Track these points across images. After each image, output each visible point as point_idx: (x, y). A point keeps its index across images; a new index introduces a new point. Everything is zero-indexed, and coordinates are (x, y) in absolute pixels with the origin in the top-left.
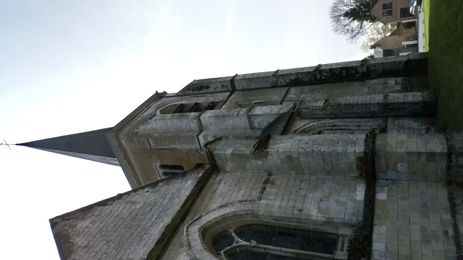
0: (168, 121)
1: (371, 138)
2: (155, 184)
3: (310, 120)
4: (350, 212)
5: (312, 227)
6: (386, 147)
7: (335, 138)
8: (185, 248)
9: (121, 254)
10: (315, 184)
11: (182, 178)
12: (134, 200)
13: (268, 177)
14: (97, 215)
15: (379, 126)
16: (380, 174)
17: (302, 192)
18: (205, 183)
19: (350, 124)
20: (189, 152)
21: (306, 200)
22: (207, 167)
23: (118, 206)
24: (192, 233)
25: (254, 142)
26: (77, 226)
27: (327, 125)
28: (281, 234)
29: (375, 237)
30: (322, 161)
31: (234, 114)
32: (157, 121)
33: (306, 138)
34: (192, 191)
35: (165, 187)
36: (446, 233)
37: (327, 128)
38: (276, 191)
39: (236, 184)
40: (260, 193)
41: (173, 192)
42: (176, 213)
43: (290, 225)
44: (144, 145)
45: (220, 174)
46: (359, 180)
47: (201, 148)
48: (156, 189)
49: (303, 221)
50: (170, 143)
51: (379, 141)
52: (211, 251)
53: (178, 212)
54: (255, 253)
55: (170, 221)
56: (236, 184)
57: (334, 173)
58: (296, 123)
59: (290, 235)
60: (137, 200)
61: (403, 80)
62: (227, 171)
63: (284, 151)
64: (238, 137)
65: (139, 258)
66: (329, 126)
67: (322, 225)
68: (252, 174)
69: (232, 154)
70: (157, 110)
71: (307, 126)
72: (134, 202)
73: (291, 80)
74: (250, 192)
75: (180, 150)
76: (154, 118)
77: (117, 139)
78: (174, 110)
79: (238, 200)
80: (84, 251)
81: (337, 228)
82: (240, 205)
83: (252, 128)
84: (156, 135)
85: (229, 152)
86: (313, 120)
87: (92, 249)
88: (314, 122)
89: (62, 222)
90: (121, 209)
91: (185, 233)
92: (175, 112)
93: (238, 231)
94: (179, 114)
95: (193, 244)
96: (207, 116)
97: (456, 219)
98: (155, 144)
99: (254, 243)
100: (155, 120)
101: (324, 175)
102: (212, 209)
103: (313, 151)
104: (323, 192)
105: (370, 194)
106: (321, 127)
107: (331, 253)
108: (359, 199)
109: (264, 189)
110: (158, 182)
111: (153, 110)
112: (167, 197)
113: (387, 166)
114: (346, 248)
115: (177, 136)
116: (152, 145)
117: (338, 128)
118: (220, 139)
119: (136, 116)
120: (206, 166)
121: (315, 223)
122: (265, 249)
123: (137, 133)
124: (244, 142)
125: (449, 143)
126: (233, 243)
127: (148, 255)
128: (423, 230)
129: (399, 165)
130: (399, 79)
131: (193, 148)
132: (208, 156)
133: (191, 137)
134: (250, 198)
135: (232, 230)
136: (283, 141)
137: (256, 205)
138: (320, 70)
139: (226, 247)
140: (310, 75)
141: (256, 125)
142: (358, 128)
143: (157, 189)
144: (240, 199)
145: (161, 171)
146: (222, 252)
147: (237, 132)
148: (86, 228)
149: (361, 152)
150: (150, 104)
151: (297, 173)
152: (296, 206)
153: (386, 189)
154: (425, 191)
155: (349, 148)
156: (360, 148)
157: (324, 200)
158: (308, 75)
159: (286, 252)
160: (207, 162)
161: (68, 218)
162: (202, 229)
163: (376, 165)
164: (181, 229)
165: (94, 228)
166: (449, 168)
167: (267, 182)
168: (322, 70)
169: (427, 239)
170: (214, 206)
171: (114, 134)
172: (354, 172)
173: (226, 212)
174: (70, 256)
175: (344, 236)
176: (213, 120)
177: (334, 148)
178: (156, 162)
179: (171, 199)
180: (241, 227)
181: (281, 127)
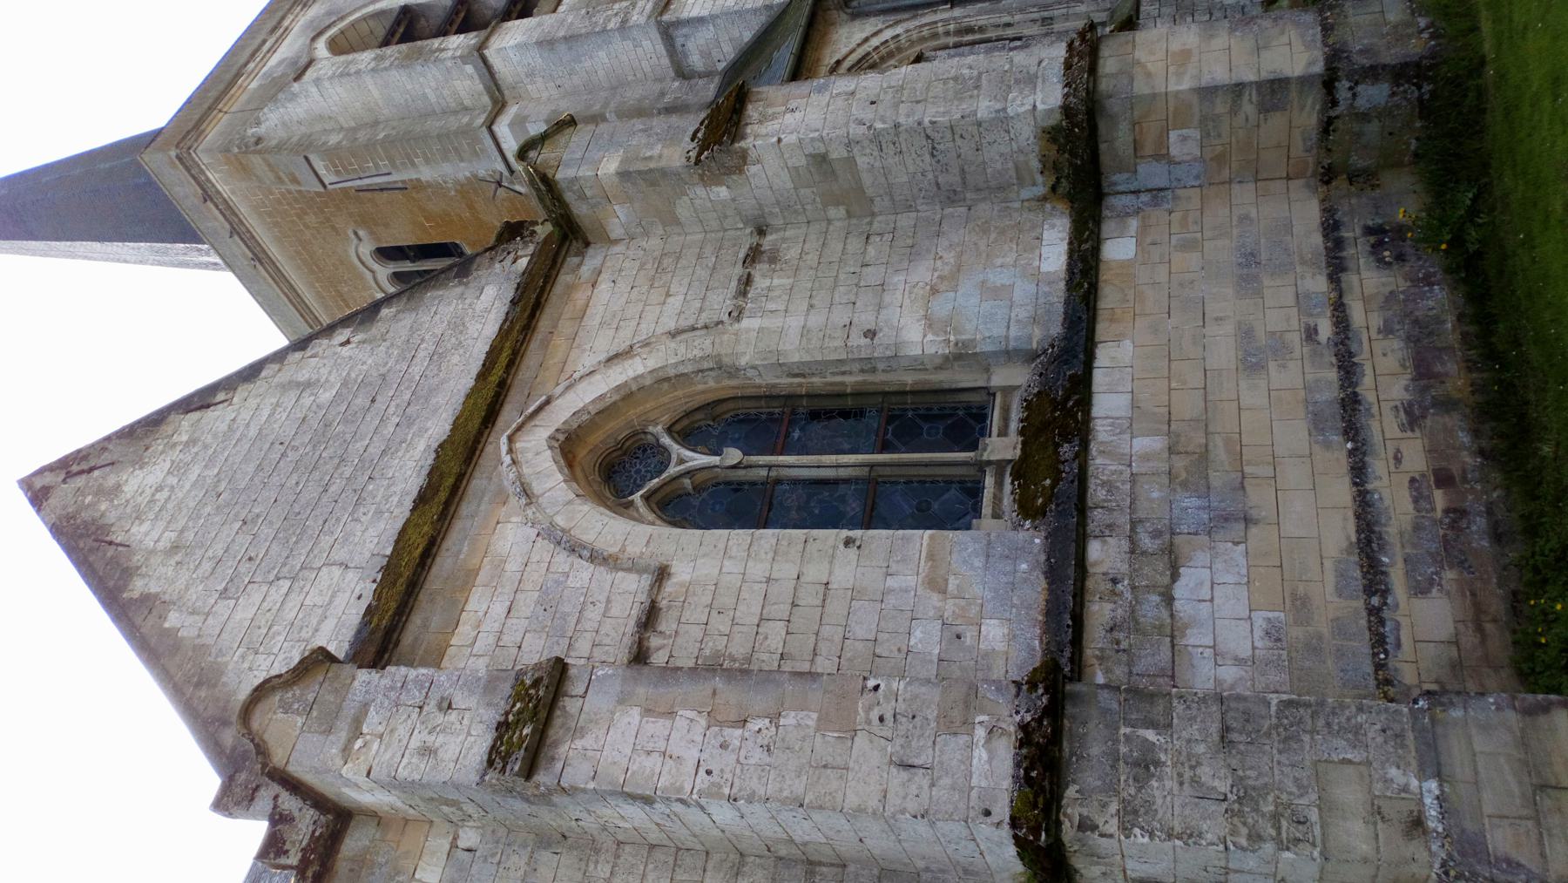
0: (368, 80)
1: (1085, 51)
2: (368, 314)
3: (882, 18)
4: (1022, 313)
5: (909, 379)
6: (1132, 80)
7: (966, 71)
8: (515, 502)
9: (304, 552)
10: (910, 242)
11: (461, 283)
12: (303, 375)
13: (755, 239)
14: (187, 444)
15: (1112, 12)
16: (1116, 178)
17: (872, 275)
18: (543, 289)
19: (1018, 17)
20: (469, 189)
21: (887, 298)
22: (543, 230)
23: (253, 403)
24: (530, 455)
25: (692, 122)
26: (125, 489)
27: (941, 30)
28: (815, 415)
29: (1099, 377)
30: (927, 157)
31: (611, 25)
32: (327, 84)
33: (870, 82)
34: (505, 321)
35: (408, 320)
36: (1311, 334)
37: (943, 41)
38: (787, 282)
39: (653, 279)
40: (735, 297)
41: (438, 332)
42: (462, 400)
43: (843, 384)
44: (295, 180)
45: (591, 251)
46: (1048, 206)
47: (512, 172)
48: (374, 330)
49: (881, 366)
50: (394, 166)
51: (1109, 63)
52: (601, 500)
53: (468, 396)
54: (740, 483)
55: (448, 427)
56: (653, 279)
57: (968, 195)
58: (835, 37)
59: (845, 414)
60: (314, 377)
62: (613, 236)
63: (800, 140)
64: (639, 112)
65: (367, 555)
66: (947, 33)
67: (939, 368)
68: (700, 236)
69: (624, 175)
70: (314, 39)
71: (875, 42)
72: (308, 384)
74: (703, 299)
75: (437, 188)
76: (310, 74)
77: (188, 169)
78: (381, 33)
79: (667, 329)
80: (173, 562)
81: (987, 370)
82: (673, 345)
83: (683, 73)
84: (333, 139)
85: (610, 166)
86: (893, 18)
87: (199, 553)
88: (897, 23)
89: (64, 481)
90: (266, 413)
91: (507, 460)
92: (386, 43)
93: (678, 427)
94: (404, 47)
95: (537, 488)
96: (512, 43)
97: (1343, 285)
98: (338, 173)
99: (733, 455)
100: (317, 81)
101: (938, 207)
102: (582, 371)
103: (897, 126)
104: (939, 263)
105: (1084, 247)
106: (922, 39)
107: (973, 446)
108: (1051, 269)
109: (748, 281)
110: (376, 307)
111: (297, 46)
112: (421, 354)
113: (1137, 146)
114: (1014, 425)
115: (411, 135)
116: (328, 178)
117: (977, 36)
118: (571, 122)
119: (238, 75)
120: (538, 229)
121: (918, 364)
122: (770, 467)
123: (259, 140)
124: (659, 124)
125: (1330, 41)
126: (667, 467)
127: (397, 542)
128: (1246, 333)
129: (1173, 135)
131: (482, 173)
132: (538, 190)
133: (466, 131)
134: (704, 318)
135: (659, 427)
136: (793, 104)
137: (726, 337)
139: (644, 480)
141: (696, 61)
142: (1044, 30)
143: (377, 329)
144: (672, 326)
145: (384, 271)
146: (637, 497)
147: (632, 95)
148: (159, 489)
149: (1051, 110)
150: (283, 18)
151: (849, 215)
152: (855, 320)
153: (1134, 224)
154: (1254, 214)
155: (1014, 100)
156: (1049, 96)
157: (942, 287)
159: (838, 466)
160: (542, 214)
161: (85, 466)
162: (562, 437)
163: (1103, 147)
164: (489, 449)
165: (187, 486)
166: (1327, 126)
167: (753, 256)
169: (1252, 363)
170: (587, 361)
171: (173, 153)
172: (1034, 184)
173: (631, 374)
174: (126, 586)
175: (1008, 391)
176: (536, 59)
177: (965, 106)
178: (355, 241)
179: (437, 357)
180: (688, 414)
181: (784, 55)
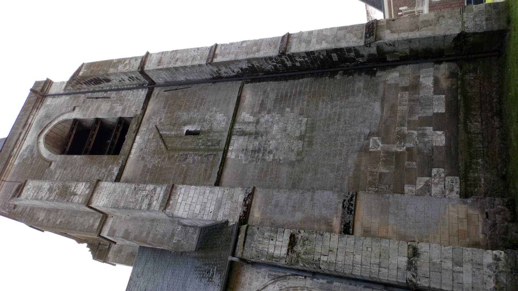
61: (452, 75)
73: (242, 69)
119: (10, 157)
130: (444, 68)
138: (289, 55)
140: (273, 62)
150: (28, 118)
158: (270, 62)
168: (293, 54)
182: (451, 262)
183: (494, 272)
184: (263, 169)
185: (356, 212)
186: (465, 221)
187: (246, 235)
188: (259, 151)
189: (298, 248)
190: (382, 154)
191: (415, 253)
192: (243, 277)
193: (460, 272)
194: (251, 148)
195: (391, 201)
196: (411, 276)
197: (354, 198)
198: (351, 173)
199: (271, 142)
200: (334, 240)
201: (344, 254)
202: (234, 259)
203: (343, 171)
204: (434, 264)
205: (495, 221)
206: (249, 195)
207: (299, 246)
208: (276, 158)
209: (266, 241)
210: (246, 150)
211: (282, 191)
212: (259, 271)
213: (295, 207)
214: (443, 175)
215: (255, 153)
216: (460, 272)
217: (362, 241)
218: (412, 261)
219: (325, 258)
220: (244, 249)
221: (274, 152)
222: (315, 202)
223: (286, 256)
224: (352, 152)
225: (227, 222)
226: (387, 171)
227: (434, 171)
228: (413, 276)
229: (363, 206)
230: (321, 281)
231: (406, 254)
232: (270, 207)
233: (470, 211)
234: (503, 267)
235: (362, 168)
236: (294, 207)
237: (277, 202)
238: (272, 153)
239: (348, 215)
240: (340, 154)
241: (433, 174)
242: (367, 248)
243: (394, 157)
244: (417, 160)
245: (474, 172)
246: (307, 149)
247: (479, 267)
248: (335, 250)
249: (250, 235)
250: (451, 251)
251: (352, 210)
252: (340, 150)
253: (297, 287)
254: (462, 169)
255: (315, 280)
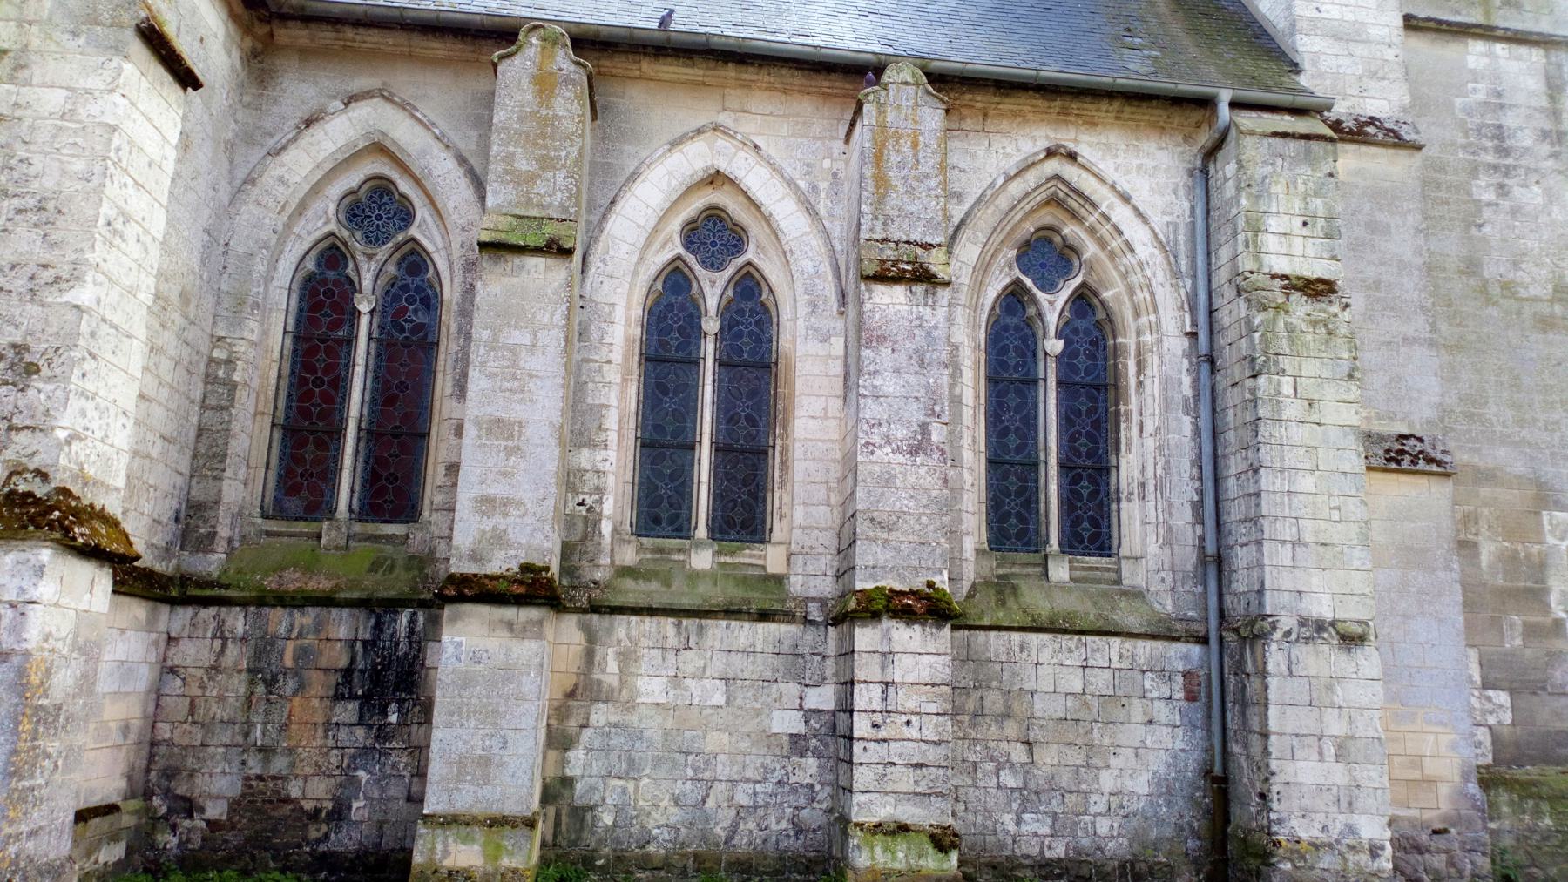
27: (1144, 320)
182: (1342, 733)
183: (1337, 841)
184: (1442, 170)
185: (1394, 476)
186: (1417, 775)
187: (1307, 137)
188: (1503, 151)
189: (1300, 307)
190: (1535, 549)
191: (1351, 640)
192: (1154, 145)
193: (1321, 754)
194: (1510, 120)
195: (1442, 574)
196: (1286, 628)
197: (1434, 468)
198: (1465, 457)
199: (1535, 189)
200: (1343, 413)
201: (1309, 443)
202: (1224, 111)
203: (1469, 431)
204: (1330, 688)
205: (1428, 851)
206: (1397, 135)
207: (1308, 308)
208: (1487, 213)
209: (1297, 205)
210: (1502, 106)
211: (1422, 242)
212: (1181, 192)
213: (1378, 289)
214: (1492, 720)
215: (1493, 137)
216: (1321, 754)
217: (1353, 492)
218: (1326, 630)
219: (1287, 389)
220: (1265, 135)
221: (1506, 204)
222: (1402, 349)
223: (1266, 270)
224: (1532, 459)
225: (1296, 68)
226: (1484, 565)
227: (1502, 698)
228: (1288, 633)
229: (1414, 494)
230: (1187, 381)
231: (1340, 615)
232: (1367, 206)
233: (1444, 790)
234: (1357, 864)
235: (1485, 491)
236: (1377, 284)
237: (1385, 230)
238: (1499, 195)
239: (1381, 452)
240: (1521, 422)
241: (1490, 693)
242: (1338, 508)
243: (1529, 584)
244: (1528, 652)
245: (1511, 803)
246: (1527, 311)
247: (1344, 804)
248: (1315, 418)
249: (1308, 152)
250: (1372, 734)
251: (1398, 462)
252: (1535, 420)
253: (1156, 311)
254: (1518, 773)
255: (1186, 362)
